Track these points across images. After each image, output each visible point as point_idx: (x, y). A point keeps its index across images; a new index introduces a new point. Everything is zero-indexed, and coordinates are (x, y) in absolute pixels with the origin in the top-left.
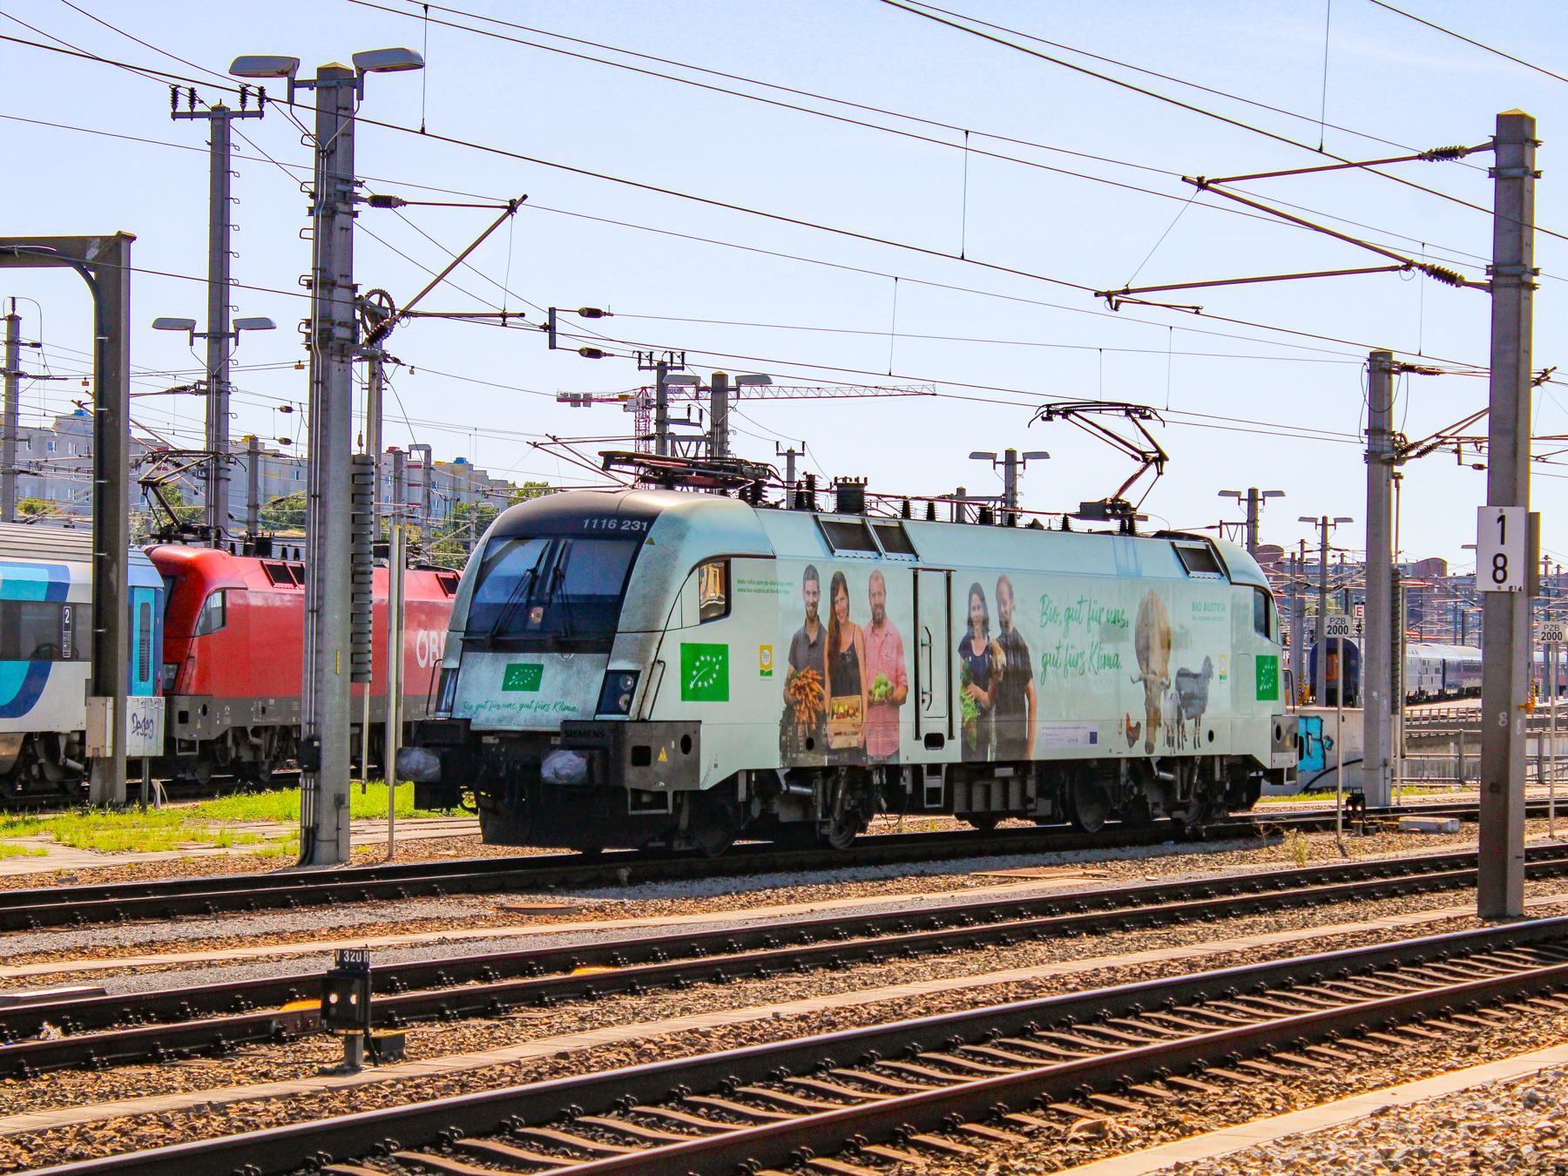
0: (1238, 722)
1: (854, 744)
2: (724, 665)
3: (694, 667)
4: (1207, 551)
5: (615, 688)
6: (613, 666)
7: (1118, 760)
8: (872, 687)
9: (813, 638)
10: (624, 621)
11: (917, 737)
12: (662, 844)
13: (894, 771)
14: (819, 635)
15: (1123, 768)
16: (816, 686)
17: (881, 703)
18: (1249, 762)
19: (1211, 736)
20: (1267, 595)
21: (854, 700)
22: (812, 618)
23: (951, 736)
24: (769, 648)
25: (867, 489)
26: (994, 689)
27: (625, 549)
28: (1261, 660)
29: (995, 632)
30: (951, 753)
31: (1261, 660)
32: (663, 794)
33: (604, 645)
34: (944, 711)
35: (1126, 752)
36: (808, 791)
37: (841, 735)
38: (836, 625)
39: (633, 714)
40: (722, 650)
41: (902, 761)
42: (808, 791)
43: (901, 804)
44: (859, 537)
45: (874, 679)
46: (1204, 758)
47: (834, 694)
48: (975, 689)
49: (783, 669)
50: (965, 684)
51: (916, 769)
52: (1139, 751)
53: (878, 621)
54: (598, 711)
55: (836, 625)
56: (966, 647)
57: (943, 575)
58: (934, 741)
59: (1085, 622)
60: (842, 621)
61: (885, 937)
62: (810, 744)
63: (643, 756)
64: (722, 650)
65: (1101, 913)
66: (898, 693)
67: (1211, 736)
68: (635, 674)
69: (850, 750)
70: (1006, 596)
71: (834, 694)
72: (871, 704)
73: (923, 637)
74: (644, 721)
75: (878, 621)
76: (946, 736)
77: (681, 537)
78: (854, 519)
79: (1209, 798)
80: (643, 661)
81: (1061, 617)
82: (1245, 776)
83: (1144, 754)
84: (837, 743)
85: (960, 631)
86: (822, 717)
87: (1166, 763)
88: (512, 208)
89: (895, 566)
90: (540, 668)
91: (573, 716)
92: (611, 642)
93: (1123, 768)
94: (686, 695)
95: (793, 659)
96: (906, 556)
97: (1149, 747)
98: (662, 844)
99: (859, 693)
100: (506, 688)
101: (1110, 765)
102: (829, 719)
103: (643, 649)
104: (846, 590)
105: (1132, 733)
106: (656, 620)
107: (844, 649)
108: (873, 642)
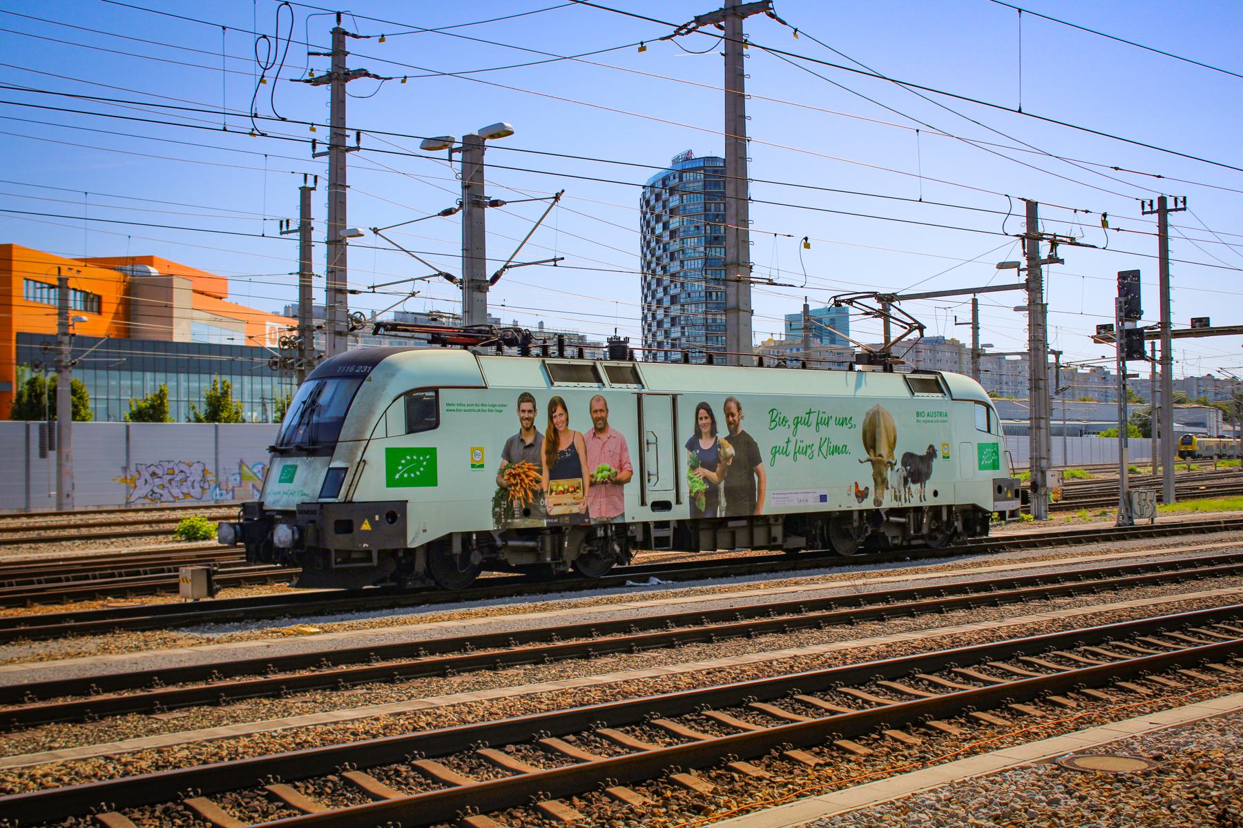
0: (962, 481)
1: (575, 510)
2: (980, 460)
3: (400, 464)
4: (937, 381)
5: (335, 479)
6: (334, 465)
7: (852, 512)
8: (595, 473)
9: (529, 440)
10: (344, 434)
11: (643, 503)
12: (394, 584)
13: (625, 526)
14: (535, 439)
15: (856, 516)
16: (533, 474)
17: (604, 483)
18: (975, 509)
19: (936, 494)
20: (988, 407)
21: (576, 481)
22: (529, 427)
23: (678, 502)
24: (482, 449)
25: (630, 345)
26: (723, 471)
27: (355, 383)
28: (981, 447)
29: (723, 432)
30: (682, 512)
31: (981, 447)
32: (369, 552)
33: (329, 451)
34: (671, 485)
35: (855, 506)
36: (902, 520)
37: (560, 501)
38: (554, 433)
39: (341, 498)
40: (432, 452)
41: (628, 520)
42: (902, 520)
43: (645, 546)
44: (591, 374)
45: (596, 465)
46: (931, 507)
47: (553, 476)
48: (703, 471)
49: (494, 462)
50: (693, 468)
51: (646, 525)
52: (868, 504)
53: (601, 426)
54: (320, 497)
55: (554, 433)
56: (692, 445)
57: (669, 399)
58: (663, 506)
59: (814, 425)
60: (561, 428)
61: (1148, 575)
62: (526, 513)
63: (346, 527)
64: (432, 452)
65: (1007, 592)
66: (622, 475)
67: (936, 494)
68: (346, 469)
69: (572, 516)
70: (734, 410)
71: (553, 476)
72: (592, 484)
73: (648, 436)
74: (351, 502)
75: (601, 426)
76: (673, 501)
77: (392, 375)
78: (626, 364)
79: (961, 530)
80: (351, 461)
81: (791, 422)
82: (975, 518)
83: (873, 507)
84: (556, 511)
85: (686, 433)
86: (539, 494)
87: (893, 512)
88: (557, 198)
89: (618, 394)
90: (296, 467)
91: (307, 500)
92: (333, 448)
93: (856, 516)
94: (391, 483)
95: (507, 454)
96: (596, 385)
97: (877, 502)
98: (394, 584)
99: (580, 475)
100: (280, 481)
101: (846, 515)
102: (547, 495)
103: (352, 452)
104: (565, 408)
105: (861, 495)
106: (363, 432)
107: (563, 446)
108: (595, 445)
